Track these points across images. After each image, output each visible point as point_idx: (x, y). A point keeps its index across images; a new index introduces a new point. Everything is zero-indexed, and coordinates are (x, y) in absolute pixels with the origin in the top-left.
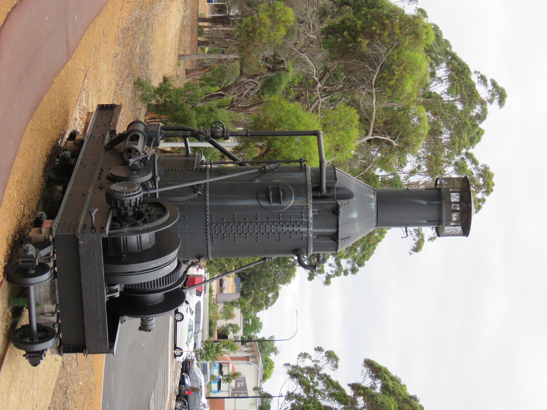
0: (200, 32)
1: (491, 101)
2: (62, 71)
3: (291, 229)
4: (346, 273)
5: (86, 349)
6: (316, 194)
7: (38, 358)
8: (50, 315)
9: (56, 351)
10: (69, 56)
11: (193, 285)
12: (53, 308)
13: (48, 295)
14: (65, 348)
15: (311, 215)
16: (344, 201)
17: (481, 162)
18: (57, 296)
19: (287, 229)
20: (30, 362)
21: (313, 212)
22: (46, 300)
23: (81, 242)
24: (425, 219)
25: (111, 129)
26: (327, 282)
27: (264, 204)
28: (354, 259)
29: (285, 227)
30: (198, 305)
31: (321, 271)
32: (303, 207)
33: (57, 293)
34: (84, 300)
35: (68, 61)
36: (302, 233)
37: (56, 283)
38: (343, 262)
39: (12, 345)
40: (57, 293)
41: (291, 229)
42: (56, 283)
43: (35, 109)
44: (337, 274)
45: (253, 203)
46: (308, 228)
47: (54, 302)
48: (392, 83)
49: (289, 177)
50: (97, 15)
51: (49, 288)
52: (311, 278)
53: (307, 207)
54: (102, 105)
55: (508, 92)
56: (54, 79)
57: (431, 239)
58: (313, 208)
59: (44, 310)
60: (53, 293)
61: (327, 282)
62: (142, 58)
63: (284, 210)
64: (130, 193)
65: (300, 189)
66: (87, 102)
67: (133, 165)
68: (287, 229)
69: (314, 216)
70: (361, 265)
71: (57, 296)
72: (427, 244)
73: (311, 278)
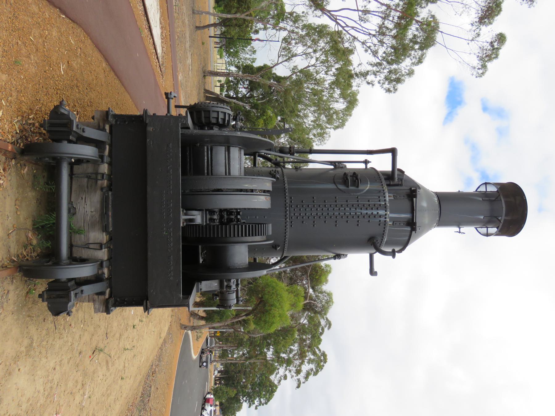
1: (325, 327)
3: (369, 212)
4: (263, 405)
5: (147, 299)
6: (388, 183)
7: (64, 300)
8: (97, 246)
9: (102, 308)
11: (209, 402)
12: (104, 238)
13: (97, 216)
14: (116, 301)
15: (387, 199)
17: (322, 350)
18: (110, 219)
19: (366, 212)
20: (50, 309)
21: (389, 197)
22: (92, 225)
23: (150, 129)
24: (481, 215)
26: (256, 408)
28: (266, 399)
29: (364, 210)
30: (211, 411)
31: (254, 403)
32: (380, 191)
33: (110, 214)
34: (149, 221)
36: (380, 216)
37: (110, 198)
38: (262, 400)
40: (110, 214)
41: (369, 212)
42: (110, 198)
44: (260, 405)
46: (386, 211)
47: (105, 229)
48: (317, 277)
51: (98, 206)
53: (384, 190)
55: (332, 323)
57: (304, 383)
58: (389, 193)
59: (88, 239)
60: (103, 214)
61: (256, 408)
63: (362, 193)
68: (366, 212)
69: (389, 200)
70: (268, 401)
71: (110, 219)
72: (302, 385)
73: (249, 407)
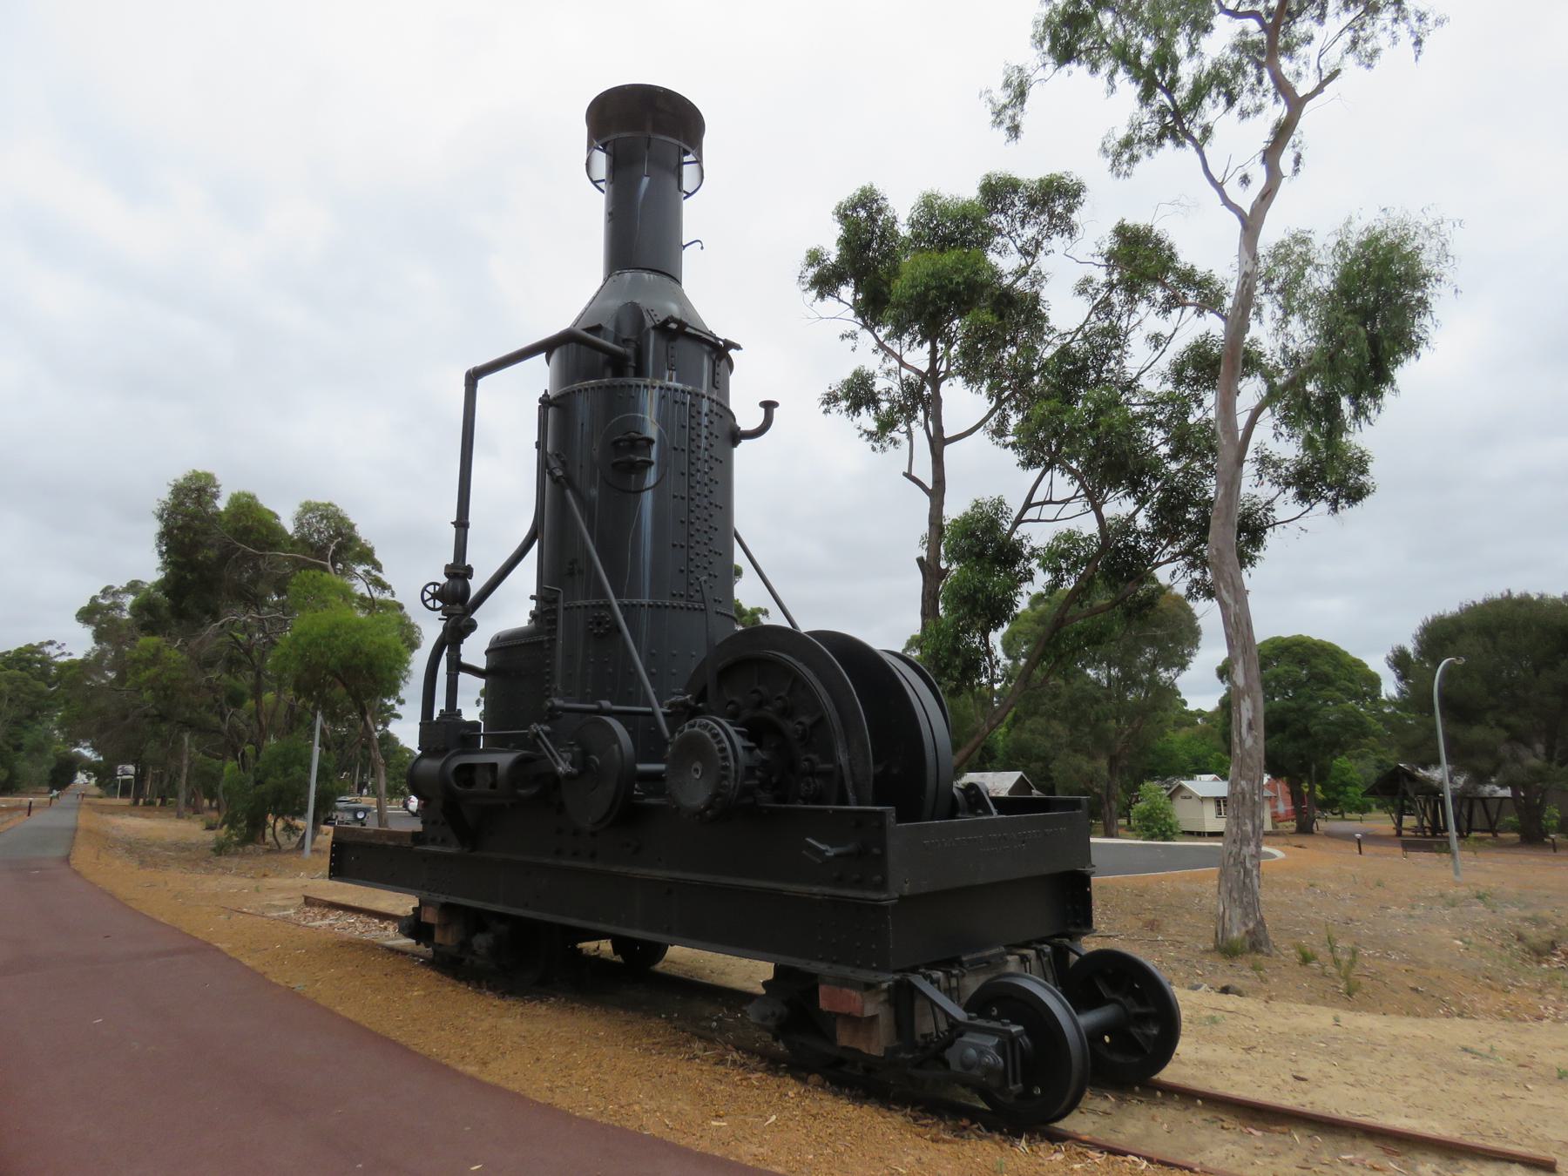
0: (151, 803)
2: (247, 962)
6: (631, 371)
10: (204, 949)
16: (647, 318)
25: (409, 843)
27: (651, 477)
35: (218, 949)
39: (1167, 1075)
43: (405, 1049)
45: (648, 499)
49: (586, 428)
50: (112, 896)
52: (398, 717)
54: (332, 869)
56: (277, 985)
62: (183, 849)
64: (723, 750)
65: (619, 403)
66: (285, 908)
67: (572, 764)
73: (398, 717)
